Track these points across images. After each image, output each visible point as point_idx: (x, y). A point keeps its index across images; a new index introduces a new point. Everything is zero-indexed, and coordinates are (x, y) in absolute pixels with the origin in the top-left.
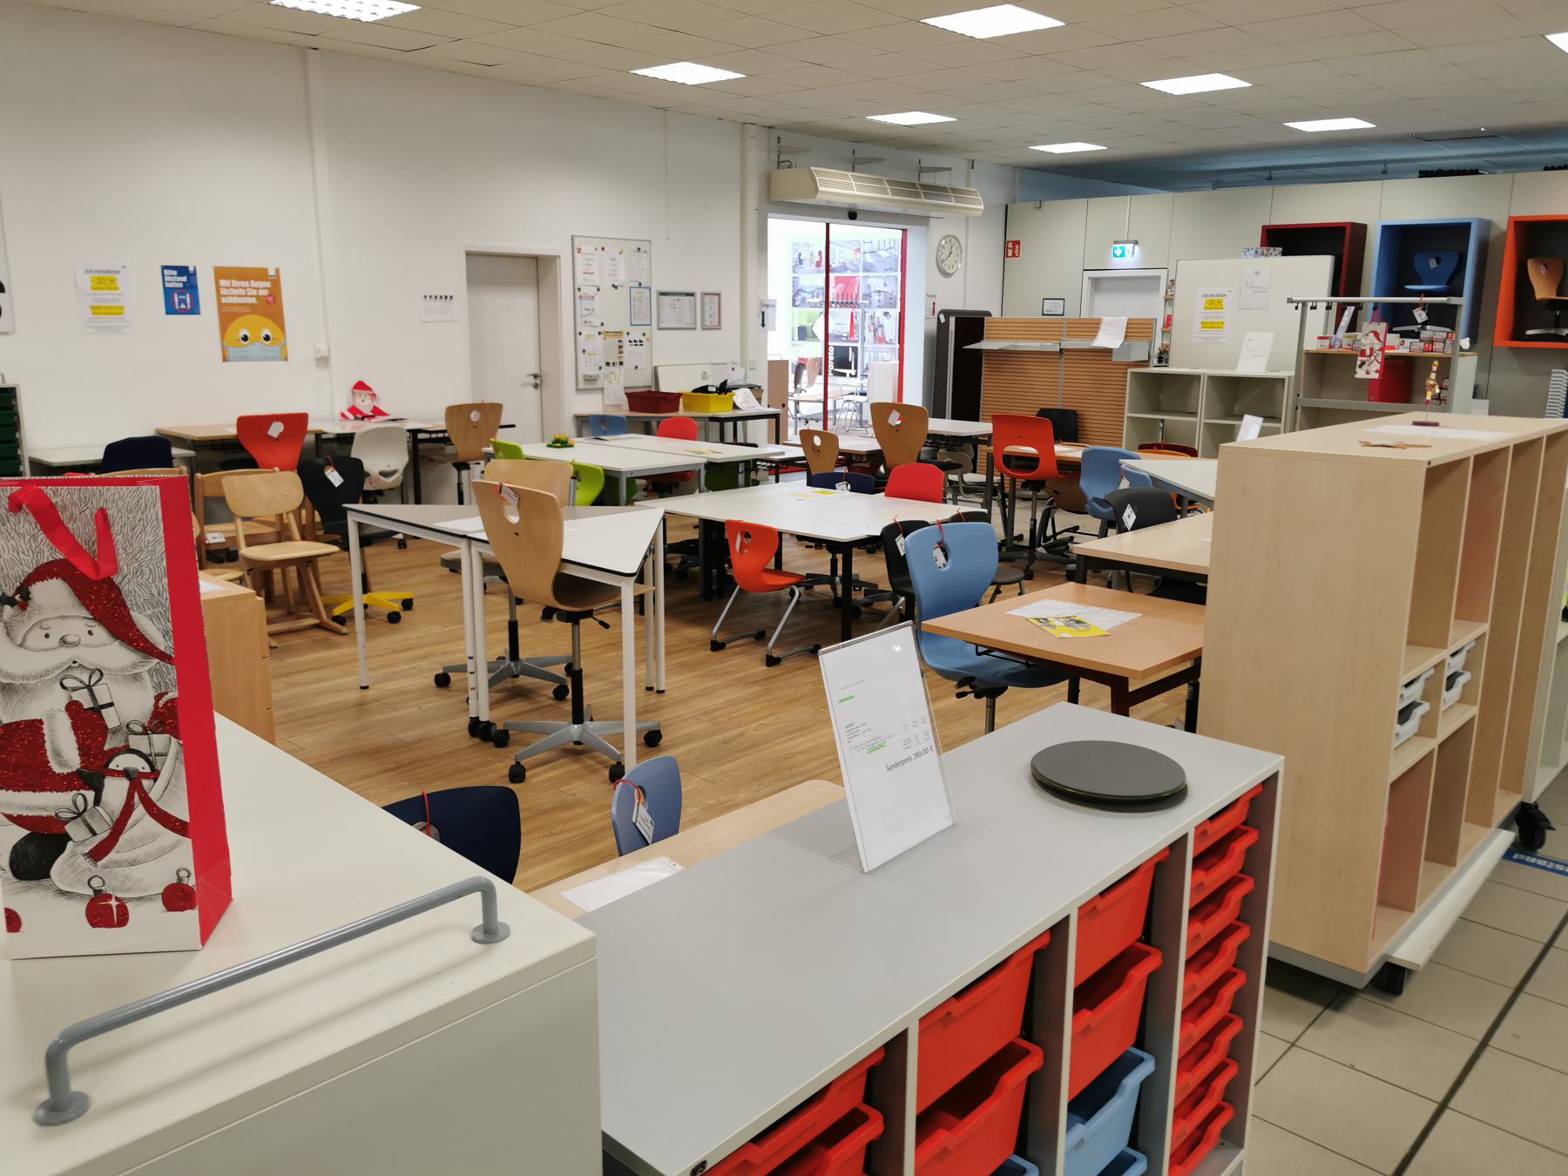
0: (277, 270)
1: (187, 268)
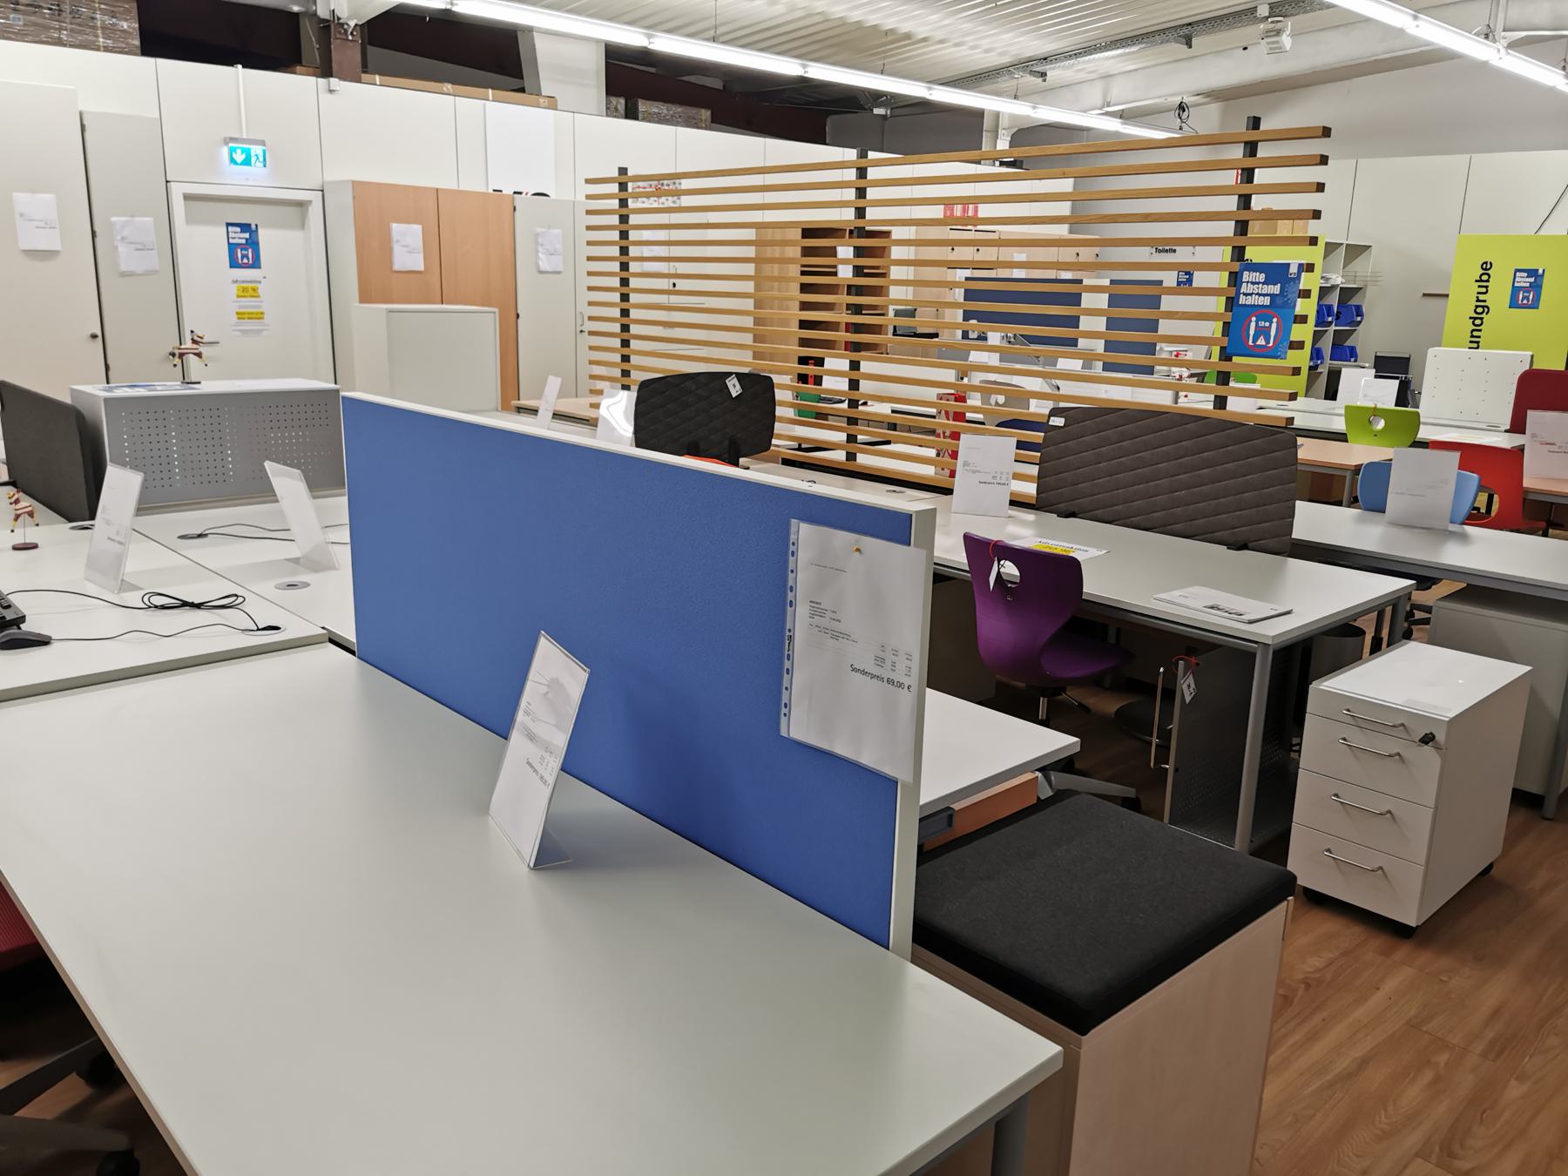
0: (257, 226)
1: (249, 225)
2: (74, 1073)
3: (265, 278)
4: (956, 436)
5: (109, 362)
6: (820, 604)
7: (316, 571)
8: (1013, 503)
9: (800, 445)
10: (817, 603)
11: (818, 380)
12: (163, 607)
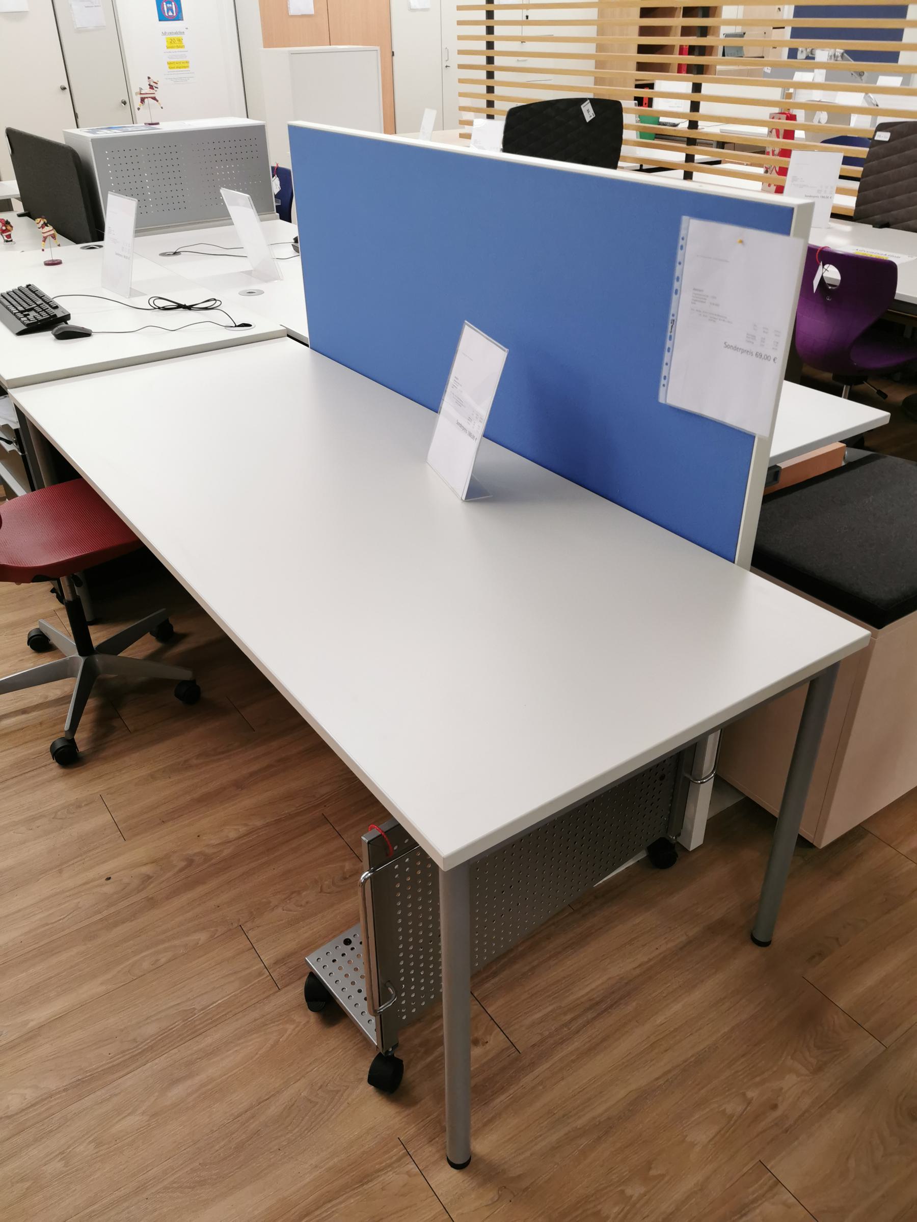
2: (149, 633)
3: (187, 28)
4: (786, 153)
5: (77, 111)
6: (702, 291)
7: (266, 281)
8: (834, 216)
9: (641, 166)
10: (700, 291)
11: (650, 103)
12: (164, 309)
